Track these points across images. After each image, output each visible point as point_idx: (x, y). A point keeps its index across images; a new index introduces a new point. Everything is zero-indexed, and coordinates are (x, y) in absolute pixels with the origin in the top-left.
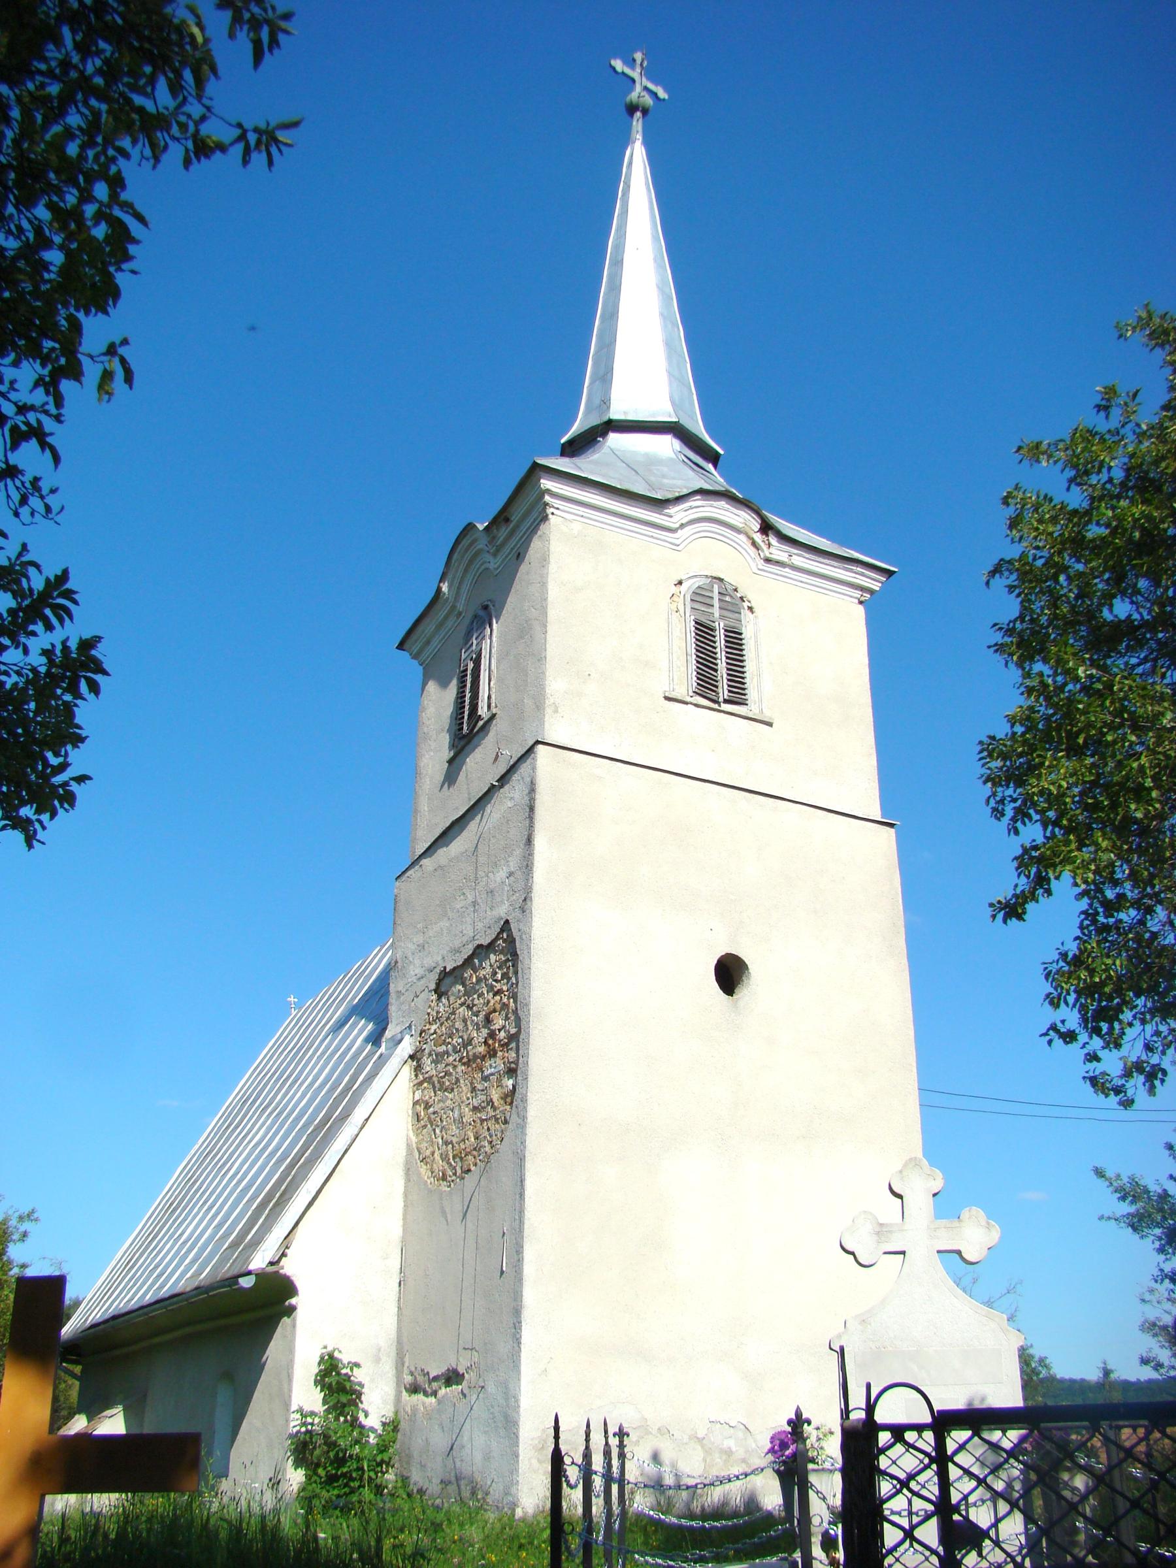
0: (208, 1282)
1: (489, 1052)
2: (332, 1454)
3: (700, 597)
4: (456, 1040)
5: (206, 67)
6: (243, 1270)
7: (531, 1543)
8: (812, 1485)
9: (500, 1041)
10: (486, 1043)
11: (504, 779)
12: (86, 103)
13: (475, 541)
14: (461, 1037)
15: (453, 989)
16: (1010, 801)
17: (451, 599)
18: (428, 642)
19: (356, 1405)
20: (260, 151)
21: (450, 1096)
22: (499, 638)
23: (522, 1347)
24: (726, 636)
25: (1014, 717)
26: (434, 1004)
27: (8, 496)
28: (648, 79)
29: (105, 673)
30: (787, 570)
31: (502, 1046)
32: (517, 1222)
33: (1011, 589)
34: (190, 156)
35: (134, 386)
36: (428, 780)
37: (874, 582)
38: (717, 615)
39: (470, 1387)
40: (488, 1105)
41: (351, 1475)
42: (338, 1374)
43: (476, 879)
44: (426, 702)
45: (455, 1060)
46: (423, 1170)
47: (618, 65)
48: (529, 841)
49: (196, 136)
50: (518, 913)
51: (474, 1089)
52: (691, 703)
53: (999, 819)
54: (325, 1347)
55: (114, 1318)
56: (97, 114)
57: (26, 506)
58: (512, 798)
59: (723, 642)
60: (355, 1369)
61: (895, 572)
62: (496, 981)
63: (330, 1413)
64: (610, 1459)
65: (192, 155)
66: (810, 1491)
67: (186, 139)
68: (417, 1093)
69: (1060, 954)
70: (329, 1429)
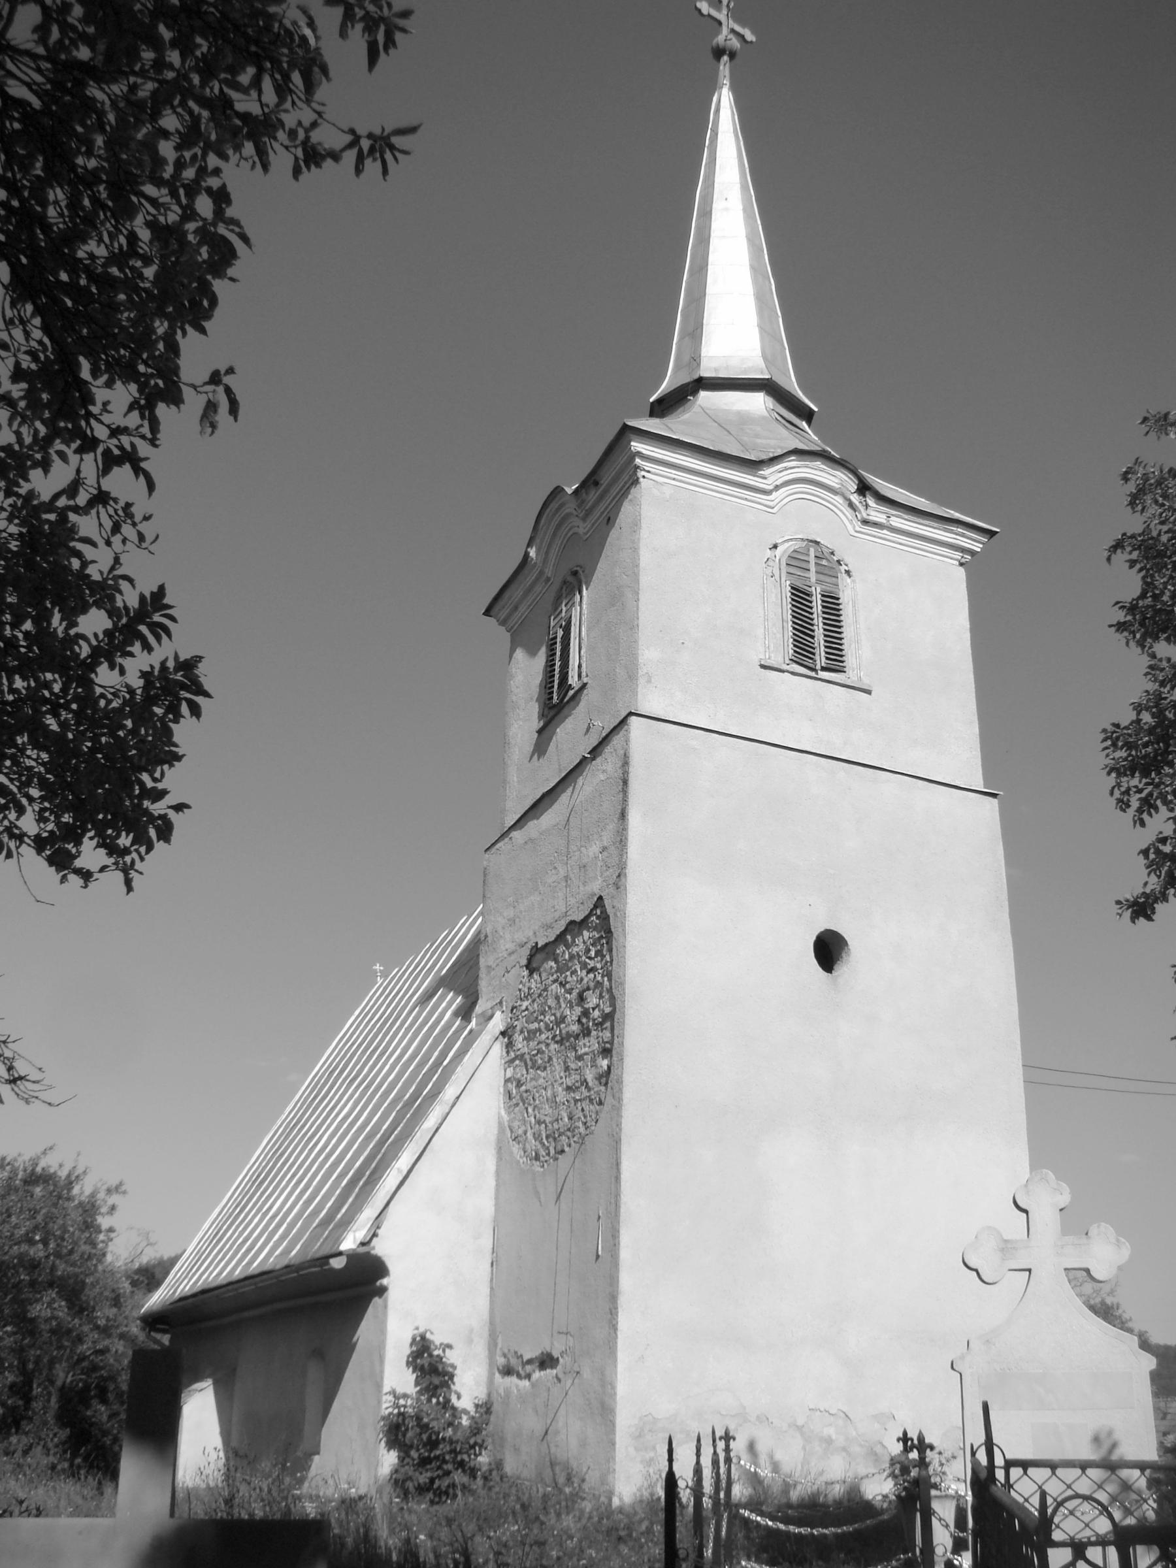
0: (297, 1261)
1: (582, 1031)
2: (425, 1437)
3: (796, 561)
4: (549, 1018)
5: (316, 69)
6: (333, 1251)
7: (630, 1535)
8: (934, 1512)
9: (594, 1020)
10: (579, 1021)
11: (596, 751)
12: (183, 104)
13: (562, 505)
14: (554, 1015)
15: (545, 965)
16: (1135, 792)
18: (516, 608)
19: (449, 1387)
20: (375, 160)
21: (543, 1074)
22: (589, 604)
23: (619, 1333)
24: (823, 601)
25: (1140, 705)
26: (525, 980)
27: (100, 525)
28: (736, 20)
29: (207, 695)
30: (885, 531)
31: (597, 1025)
32: (614, 1205)
33: (1132, 563)
34: (300, 166)
35: (239, 418)
36: (517, 750)
37: (975, 543)
38: (813, 580)
39: (565, 1373)
40: (582, 1085)
41: (444, 1458)
42: (431, 1355)
44: (514, 670)
45: (548, 1038)
46: (516, 1149)
48: (623, 815)
49: (306, 142)
50: (612, 890)
51: (567, 1069)
52: (788, 672)
53: (1124, 811)
54: (417, 1328)
55: (204, 1292)
56: (196, 119)
57: (119, 535)
58: (604, 771)
59: (820, 608)
60: (447, 1351)
61: (997, 532)
62: (590, 958)
63: (423, 1395)
64: (719, 1468)
65: (302, 164)
66: (933, 1518)
67: (296, 147)
68: (508, 1070)
70: (422, 1411)
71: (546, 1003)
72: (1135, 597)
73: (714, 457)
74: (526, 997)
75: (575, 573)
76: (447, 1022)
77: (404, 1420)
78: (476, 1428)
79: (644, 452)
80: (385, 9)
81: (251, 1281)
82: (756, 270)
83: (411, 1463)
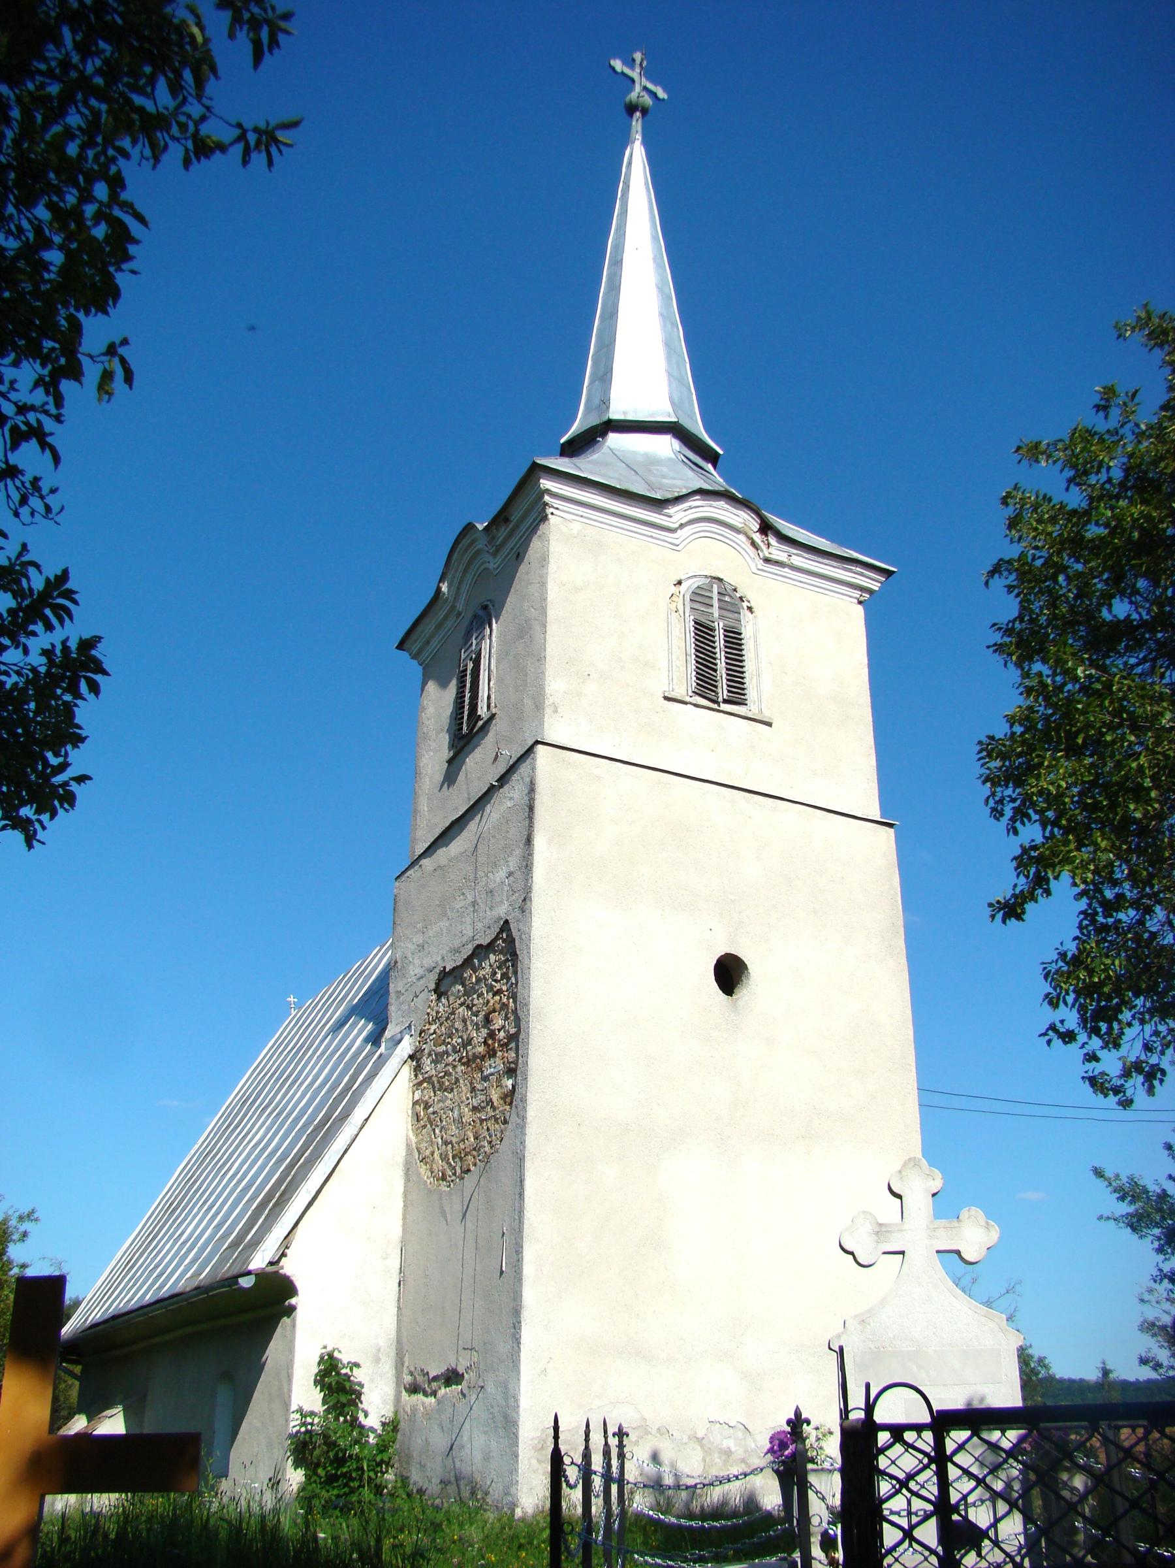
0: (208, 1282)
1: (488, 1053)
2: (331, 1454)
3: (699, 597)
4: (456, 1040)
5: (205, 67)
6: (243, 1270)
7: (531, 1543)
8: (811, 1485)
10: (485, 1043)
11: (503, 779)
13: (474, 541)
14: (461, 1037)
15: (453, 989)
16: (1009, 802)
17: (451, 599)
18: (427, 643)
19: (356, 1405)
20: (260, 152)
21: (450, 1096)
22: (498, 638)
23: (522, 1347)
25: (1013, 717)
27: (8, 496)
28: (647, 79)
29: (105, 673)
30: (786, 570)
31: (502, 1046)
32: (517, 1222)
33: (1010, 589)
34: (190, 156)
35: (134, 387)
36: (427, 780)
37: (873, 583)
38: (716, 615)
39: (469, 1387)
40: (488, 1105)
41: (351, 1475)
42: (338, 1374)
43: (476, 878)
45: (454, 1060)
46: (423, 1170)
47: (618, 65)
48: (529, 841)
50: (517, 913)
51: (473, 1089)
52: (691, 703)
53: (998, 819)
54: (325, 1347)
55: (114, 1318)
57: (26, 507)
58: (511, 798)
59: (722, 642)
61: (894, 572)
62: (496, 981)
63: (330, 1413)
64: (610, 1459)
65: (192, 155)
67: (186, 139)
69: (1059, 954)
70: (329, 1428)
71: (453, 1026)
72: (1012, 619)
73: (620, 495)
74: (434, 1021)
75: (485, 608)
76: (358, 1048)
77: (311, 1438)
78: (382, 1446)
79: (553, 489)
80: (270, 12)
81: (162, 1304)
82: (665, 317)
83: (318, 1481)
